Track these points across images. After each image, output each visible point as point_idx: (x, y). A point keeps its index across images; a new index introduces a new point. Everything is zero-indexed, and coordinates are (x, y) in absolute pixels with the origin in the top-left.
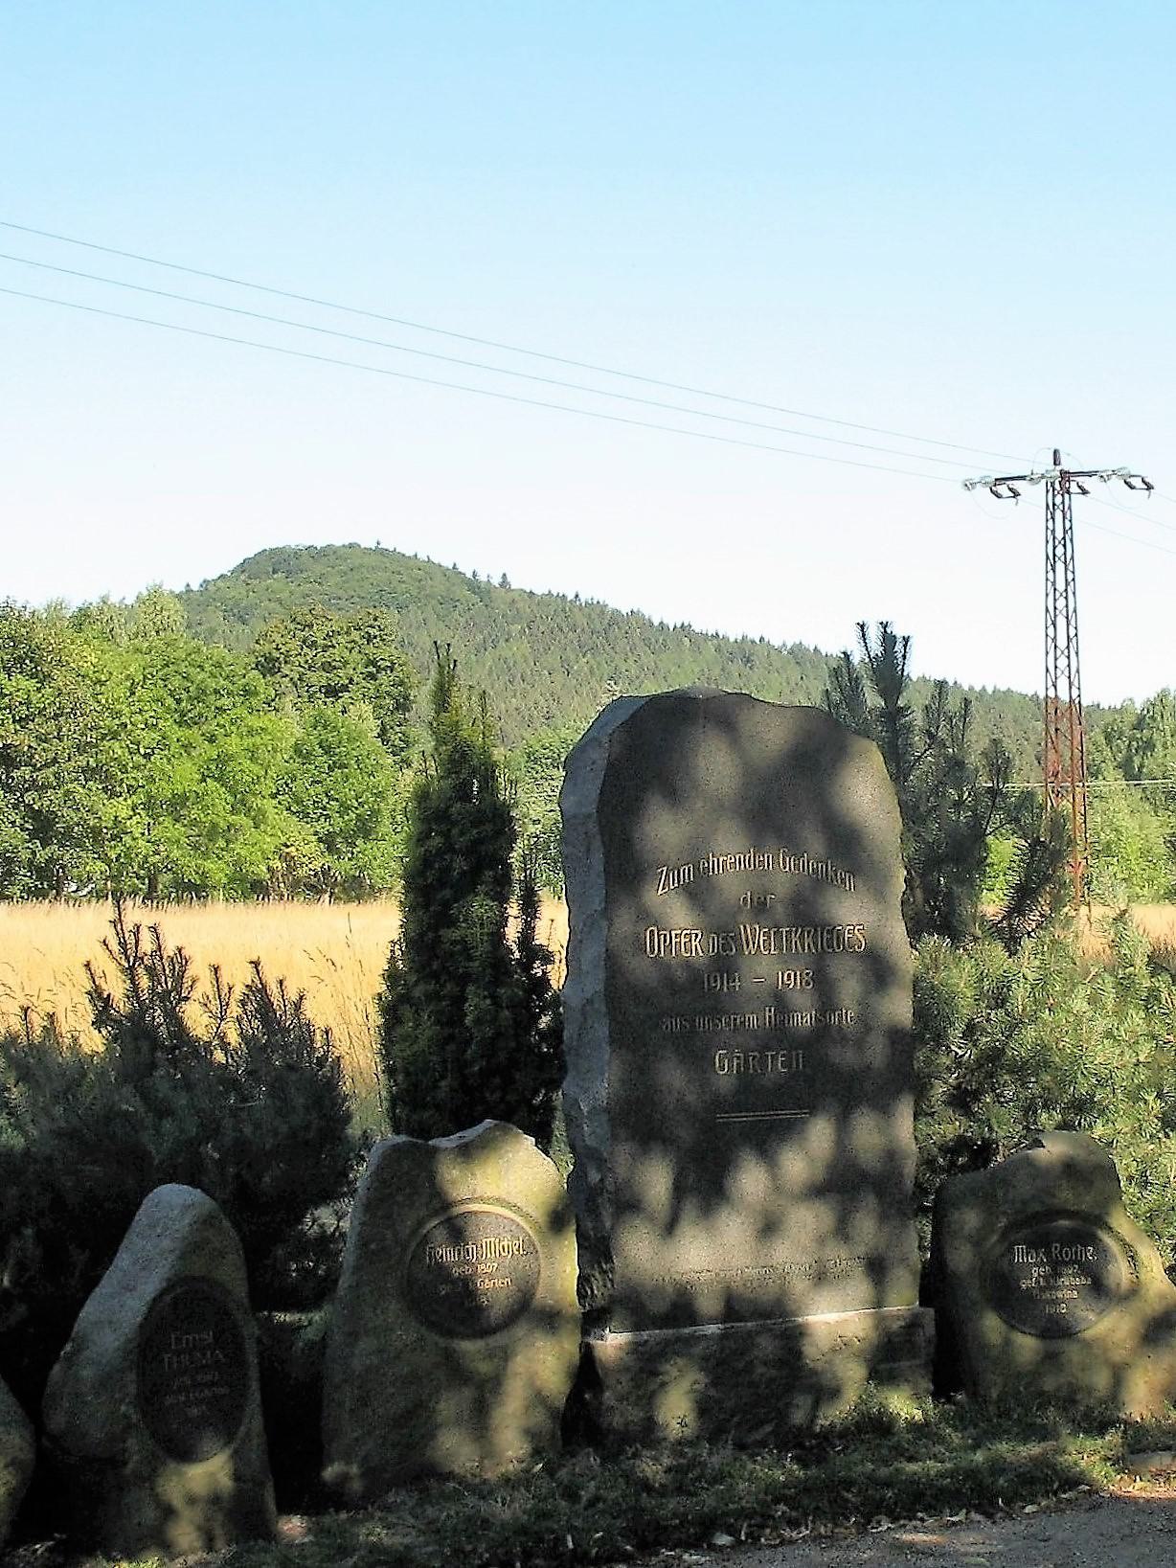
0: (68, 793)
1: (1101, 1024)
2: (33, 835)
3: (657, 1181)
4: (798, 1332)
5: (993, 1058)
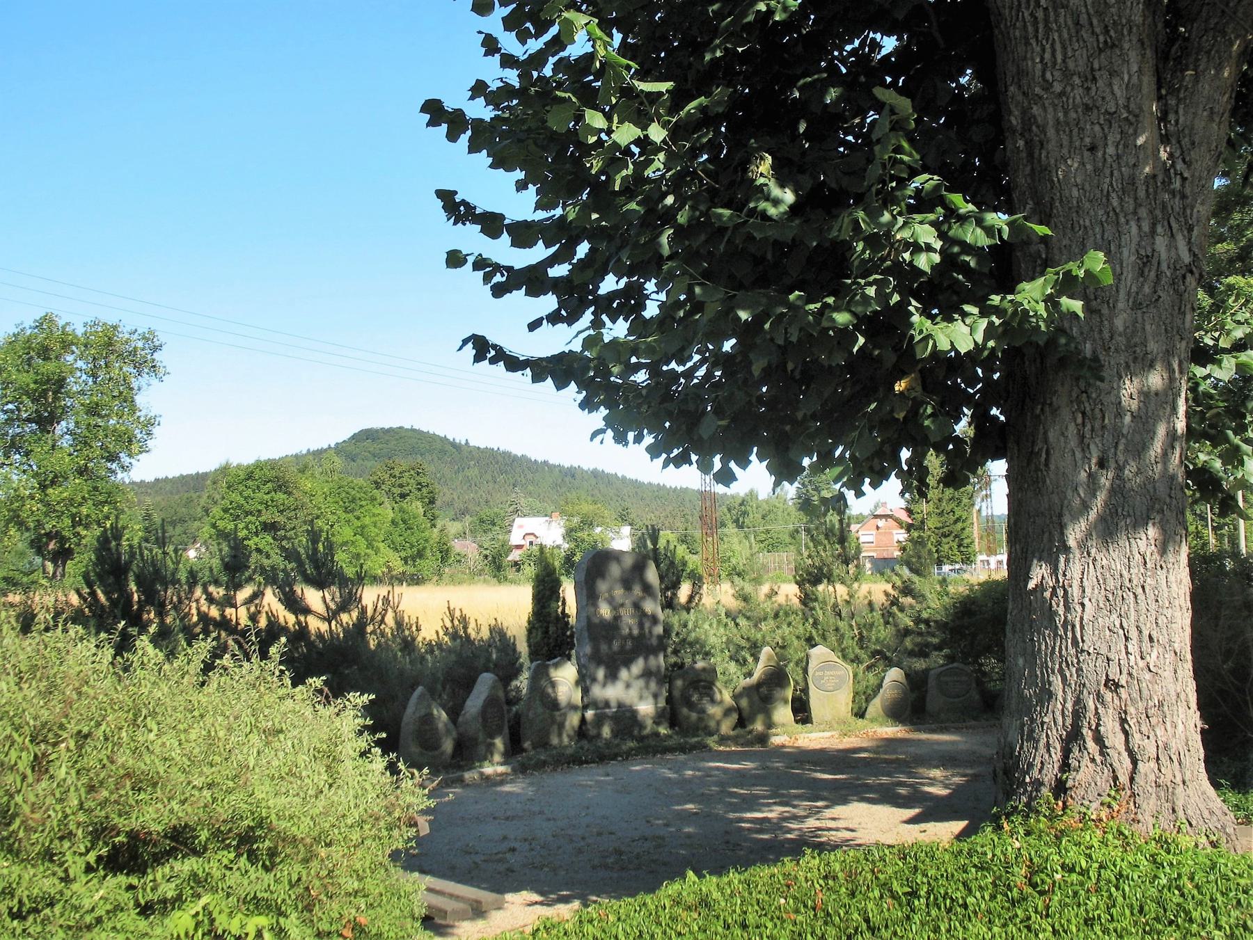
0: (300, 541)
1: (712, 632)
2: (286, 558)
3: (601, 673)
4: (800, 501)
5: (684, 640)
